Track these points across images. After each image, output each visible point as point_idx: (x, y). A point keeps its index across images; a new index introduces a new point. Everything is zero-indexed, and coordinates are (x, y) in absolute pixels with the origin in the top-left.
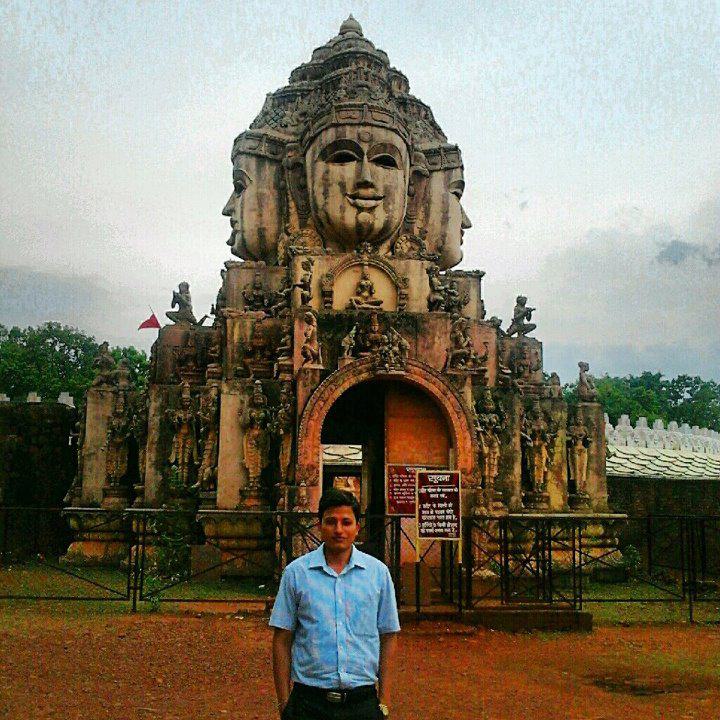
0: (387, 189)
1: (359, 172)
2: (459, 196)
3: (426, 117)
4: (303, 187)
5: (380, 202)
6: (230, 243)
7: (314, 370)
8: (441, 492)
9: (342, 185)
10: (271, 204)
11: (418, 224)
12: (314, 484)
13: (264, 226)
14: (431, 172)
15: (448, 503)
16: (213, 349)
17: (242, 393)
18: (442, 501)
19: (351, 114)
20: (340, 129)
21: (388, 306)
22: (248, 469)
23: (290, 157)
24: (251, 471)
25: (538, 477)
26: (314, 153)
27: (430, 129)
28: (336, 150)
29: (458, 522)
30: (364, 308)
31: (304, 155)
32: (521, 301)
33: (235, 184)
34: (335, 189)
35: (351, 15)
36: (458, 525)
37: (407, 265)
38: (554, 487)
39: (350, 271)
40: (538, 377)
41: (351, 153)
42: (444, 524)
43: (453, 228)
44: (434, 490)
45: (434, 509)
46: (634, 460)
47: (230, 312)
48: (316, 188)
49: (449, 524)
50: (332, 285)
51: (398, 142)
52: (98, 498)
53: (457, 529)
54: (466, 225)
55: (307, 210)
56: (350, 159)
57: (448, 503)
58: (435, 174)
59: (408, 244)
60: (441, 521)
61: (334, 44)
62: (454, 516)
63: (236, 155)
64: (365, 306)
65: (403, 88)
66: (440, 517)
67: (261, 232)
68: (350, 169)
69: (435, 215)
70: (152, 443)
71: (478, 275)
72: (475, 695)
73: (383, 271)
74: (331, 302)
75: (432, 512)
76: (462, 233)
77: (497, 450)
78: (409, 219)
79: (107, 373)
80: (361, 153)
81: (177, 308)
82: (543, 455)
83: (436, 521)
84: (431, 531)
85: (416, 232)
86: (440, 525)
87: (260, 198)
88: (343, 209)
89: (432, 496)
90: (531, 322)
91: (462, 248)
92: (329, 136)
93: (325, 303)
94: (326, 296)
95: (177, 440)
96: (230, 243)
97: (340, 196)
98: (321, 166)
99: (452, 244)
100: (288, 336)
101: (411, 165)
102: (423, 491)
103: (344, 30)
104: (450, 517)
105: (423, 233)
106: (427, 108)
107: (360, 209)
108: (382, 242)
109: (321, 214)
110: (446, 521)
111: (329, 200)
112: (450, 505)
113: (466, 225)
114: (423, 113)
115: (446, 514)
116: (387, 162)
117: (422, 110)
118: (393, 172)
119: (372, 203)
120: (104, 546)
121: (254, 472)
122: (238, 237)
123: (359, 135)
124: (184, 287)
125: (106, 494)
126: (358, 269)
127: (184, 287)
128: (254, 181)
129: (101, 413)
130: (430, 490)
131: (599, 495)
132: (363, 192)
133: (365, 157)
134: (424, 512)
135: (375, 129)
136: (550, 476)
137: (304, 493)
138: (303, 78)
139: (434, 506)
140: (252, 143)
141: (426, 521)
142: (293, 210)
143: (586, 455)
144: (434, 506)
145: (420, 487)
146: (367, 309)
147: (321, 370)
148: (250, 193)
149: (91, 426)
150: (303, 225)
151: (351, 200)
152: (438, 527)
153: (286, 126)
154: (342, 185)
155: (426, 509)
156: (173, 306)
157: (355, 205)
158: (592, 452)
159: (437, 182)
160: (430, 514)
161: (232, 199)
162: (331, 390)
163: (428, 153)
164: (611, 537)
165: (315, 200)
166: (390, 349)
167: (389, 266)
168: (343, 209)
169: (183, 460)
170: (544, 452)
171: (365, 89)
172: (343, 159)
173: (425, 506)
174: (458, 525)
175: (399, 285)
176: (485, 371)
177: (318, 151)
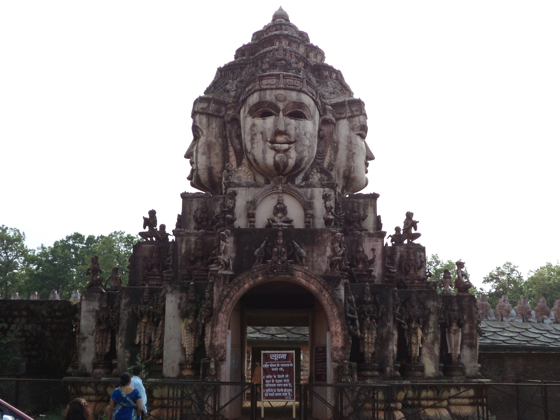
1: (275, 124)
2: (363, 137)
3: (337, 79)
4: (239, 136)
5: (292, 145)
6: (189, 178)
7: (225, 276)
8: (280, 367)
10: (217, 149)
12: (223, 360)
13: (212, 165)
14: (338, 119)
15: (285, 375)
16: (168, 259)
17: (181, 292)
18: (279, 373)
19: (270, 81)
20: (262, 93)
21: (299, 223)
22: (185, 349)
24: (187, 349)
25: (415, 350)
26: (245, 110)
27: (339, 87)
29: (293, 388)
30: (278, 226)
31: (239, 113)
32: (409, 215)
33: (194, 135)
34: (259, 136)
35: (281, 7)
36: (293, 390)
37: (312, 191)
38: (429, 360)
40: (421, 273)
41: (270, 110)
42: (282, 390)
43: (360, 160)
44: (275, 365)
45: (275, 379)
46: (526, 334)
48: (246, 138)
49: (285, 390)
51: (307, 100)
52: (89, 369)
53: (292, 393)
54: (370, 157)
55: (241, 153)
56: (269, 114)
57: (285, 375)
59: (319, 175)
60: (280, 388)
61: (268, 28)
62: (290, 384)
63: (194, 114)
64: (280, 224)
65: (319, 57)
66: (279, 385)
67: (210, 170)
68: (270, 120)
69: (342, 154)
70: (122, 330)
71: (374, 197)
73: (296, 198)
74: (254, 222)
75: (273, 381)
76: (367, 165)
77: (375, 332)
78: (321, 154)
80: (278, 110)
81: (147, 229)
82: (419, 335)
83: (276, 387)
84: (272, 395)
85: (326, 165)
86: (279, 390)
88: (264, 152)
89: (273, 369)
90: (417, 232)
91: (366, 175)
92: (254, 99)
94: (251, 216)
95: (141, 326)
96: (189, 178)
97: (261, 142)
99: (359, 173)
101: (320, 116)
102: (266, 366)
103: (276, 17)
104: (287, 385)
105: (331, 166)
106: (338, 73)
107: (277, 151)
108: (297, 175)
109: (250, 157)
110: (284, 388)
111: (255, 146)
112: (287, 376)
113: (370, 157)
114: (334, 76)
115: (283, 383)
117: (337, 76)
118: (302, 122)
119: (286, 146)
120: (93, 404)
121: (189, 351)
122: (195, 174)
123: (276, 97)
124: (152, 213)
125: (95, 366)
127: (152, 213)
129: (91, 307)
130: (271, 365)
131: (473, 364)
133: (281, 113)
134: (267, 381)
135: (288, 91)
136: (425, 350)
137: (212, 366)
138: (243, 55)
139: (275, 377)
140: (204, 105)
141: (269, 387)
143: (460, 334)
144: (275, 377)
145: (264, 364)
146: (281, 226)
147: (230, 275)
148: (202, 140)
149: (84, 317)
150: (239, 164)
152: (277, 392)
155: (269, 379)
156: (145, 228)
157: (273, 149)
158: (466, 332)
159: (343, 127)
160: (271, 383)
161: (192, 146)
162: (236, 289)
164: (481, 397)
165: (245, 146)
166: (279, 258)
167: (298, 192)
168: (264, 152)
169: (144, 342)
170: (420, 332)
172: (265, 115)
173: (267, 377)
174: (293, 390)
175: (307, 206)
176: (372, 271)
177: (247, 109)
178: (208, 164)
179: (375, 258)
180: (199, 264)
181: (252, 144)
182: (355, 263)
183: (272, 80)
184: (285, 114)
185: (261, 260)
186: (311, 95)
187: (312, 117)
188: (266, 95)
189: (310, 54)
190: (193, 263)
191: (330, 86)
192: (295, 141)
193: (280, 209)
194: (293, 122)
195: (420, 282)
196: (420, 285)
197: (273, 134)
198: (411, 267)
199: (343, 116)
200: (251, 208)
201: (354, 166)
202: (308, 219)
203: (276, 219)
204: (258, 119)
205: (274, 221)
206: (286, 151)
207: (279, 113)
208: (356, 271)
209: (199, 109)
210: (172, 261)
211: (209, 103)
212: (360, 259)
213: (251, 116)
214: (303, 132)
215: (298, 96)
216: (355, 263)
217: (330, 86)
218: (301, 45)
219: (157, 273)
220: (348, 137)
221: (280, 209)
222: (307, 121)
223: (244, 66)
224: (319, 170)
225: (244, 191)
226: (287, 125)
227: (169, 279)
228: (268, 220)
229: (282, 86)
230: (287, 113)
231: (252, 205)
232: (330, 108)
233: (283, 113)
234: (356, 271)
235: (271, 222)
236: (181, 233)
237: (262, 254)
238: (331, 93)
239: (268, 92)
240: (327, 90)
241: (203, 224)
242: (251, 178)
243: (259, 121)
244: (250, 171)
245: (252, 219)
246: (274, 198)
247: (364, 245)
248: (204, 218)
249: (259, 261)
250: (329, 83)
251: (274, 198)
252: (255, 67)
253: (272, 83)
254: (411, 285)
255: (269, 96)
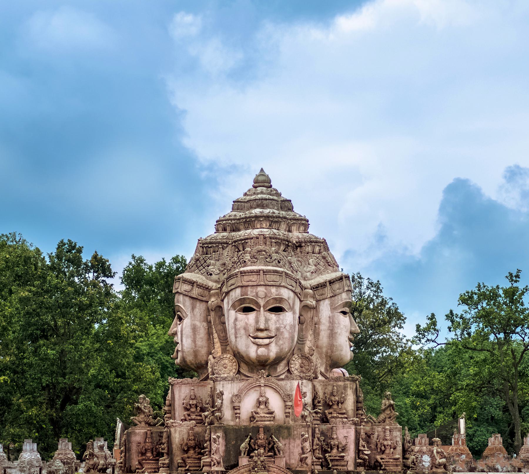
0: (278, 329)
1: (257, 321)
5: (272, 339)
9: (246, 329)
10: (202, 333)
11: (309, 344)
20: (244, 288)
23: (213, 301)
28: (242, 304)
34: (242, 332)
39: (252, 390)
47: (173, 423)
50: (240, 402)
51: (286, 293)
55: (225, 341)
58: (322, 303)
68: (252, 316)
72: (76, 376)
79: (70, 466)
80: (259, 306)
85: (307, 349)
87: (194, 329)
92: (237, 294)
93: (236, 414)
98: (233, 313)
100: (208, 443)
111: (238, 339)
116: (278, 310)
118: (282, 315)
119: (267, 341)
126: (257, 389)
128: (189, 315)
132: (260, 334)
133: (262, 308)
142: (216, 340)
150: (224, 351)
151: (252, 339)
153: (211, 274)
154: (246, 329)
163: (315, 288)
167: (278, 385)
168: (247, 347)
171: (264, 253)
172: (247, 310)
178: (194, 347)
179: (347, 445)
180: (192, 452)
181: (236, 337)
182: (329, 450)
183: (253, 276)
184: (265, 310)
185: (246, 454)
186: (290, 287)
187: (292, 309)
188: (247, 292)
189: (293, 227)
190: (186, 452)
191: (312, 264)
192: (276, 335)
193: (262, 403)
194: (273, 316)
195: (395, 461)
196: (395, 463)
197: (248, 396)
198: (387, 447)
199: (324, 297)
200: (237, 401)
201: (336, 345)
202: (287, 410)
203: (259, 410)
204: (240, 314)
205: (257, 413)
206: (267, 345)
207: (260, 308)
208: (330, 456)
209: (182, 290)
210: (166, 449)
211: (193, 286)
212: (334, 445)
213: (235, 310)
214: (282, 326)
215: (277, 291)
216: (329, 450)
217: (312, 264)
218: (282, 245)
219: (151, 458)
220: (330, 317)
221: (262, 403)
222: (287, 313)
223: (225, 245)
224: (300, 355)
225: (230, 385)
226: (267, 320)
227: (165, 466)
228: (252, 412)
229: (262, 283)
230: (268, 309)
231: (238, 397)
232: (311, 291)
233: (264, 309)
234: (330, 456)
235: (255, 414)
236: (174, 424)
237: (247, 448)
238: (312, 273)
239: (249, 289)
240: (308, 270)
241: (192, 410)
242: (236, 366)
243: (241, 316)
244: (234, 358)
245: (238, 411)
246: (257, 390)
247: (338, 432)
248: (193, 405)
249: (244, 454)
250: (311, 261)
251: (257, 390)
252: (236, 252)
253: (253, 279)
254: (387, 463)
255: (251, 294)
